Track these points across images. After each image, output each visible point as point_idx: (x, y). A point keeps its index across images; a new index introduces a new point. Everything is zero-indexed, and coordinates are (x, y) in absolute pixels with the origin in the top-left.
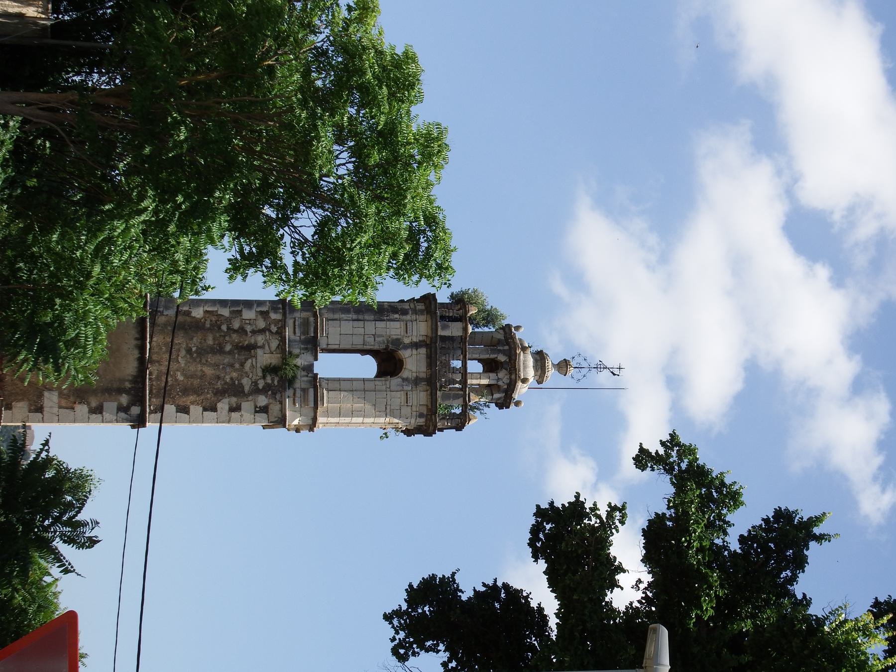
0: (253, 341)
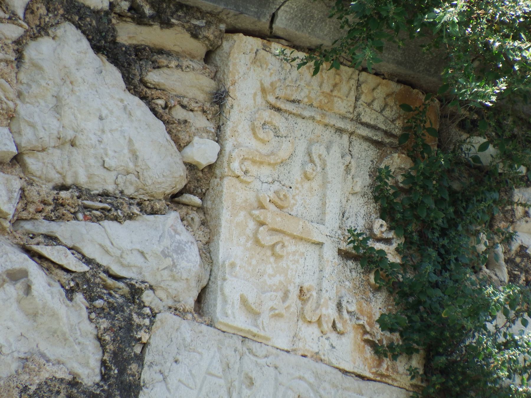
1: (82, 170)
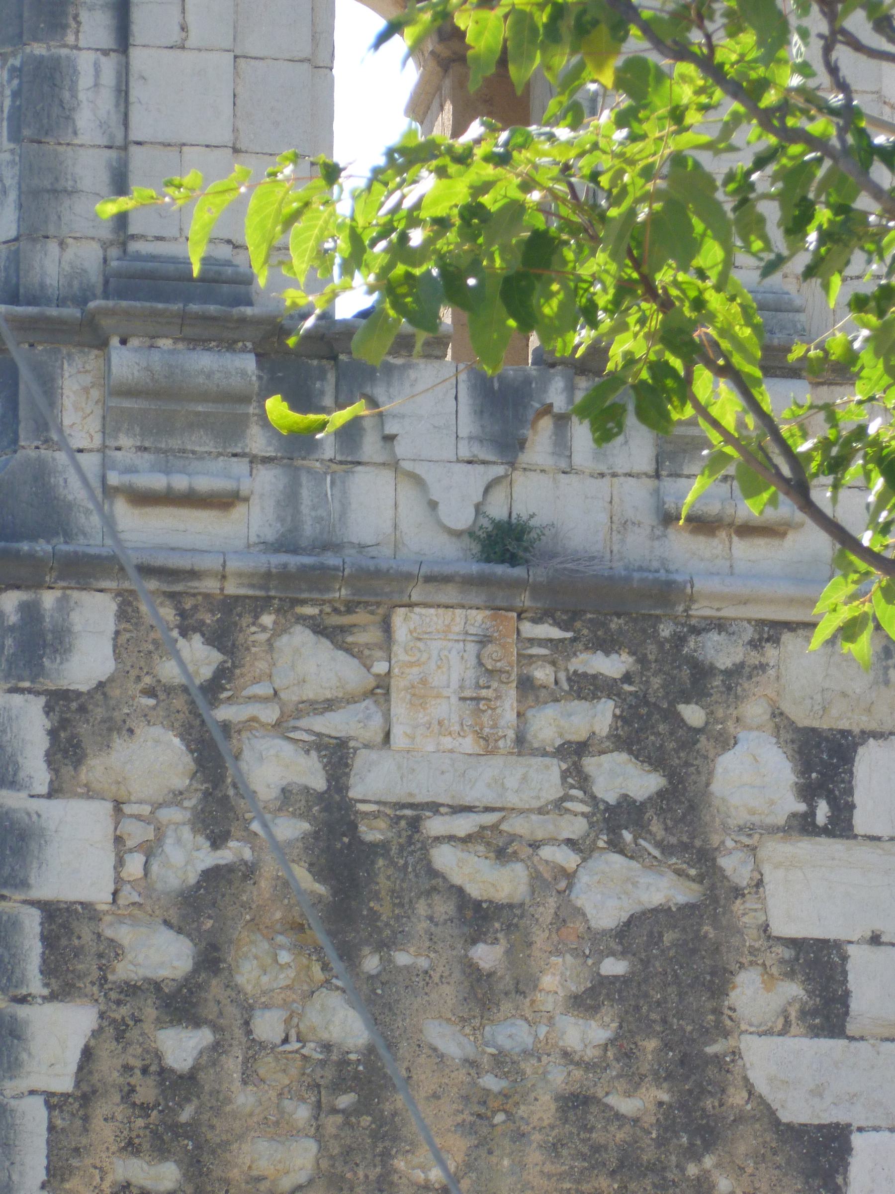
0: (290, 829)
1: (309, 693)
